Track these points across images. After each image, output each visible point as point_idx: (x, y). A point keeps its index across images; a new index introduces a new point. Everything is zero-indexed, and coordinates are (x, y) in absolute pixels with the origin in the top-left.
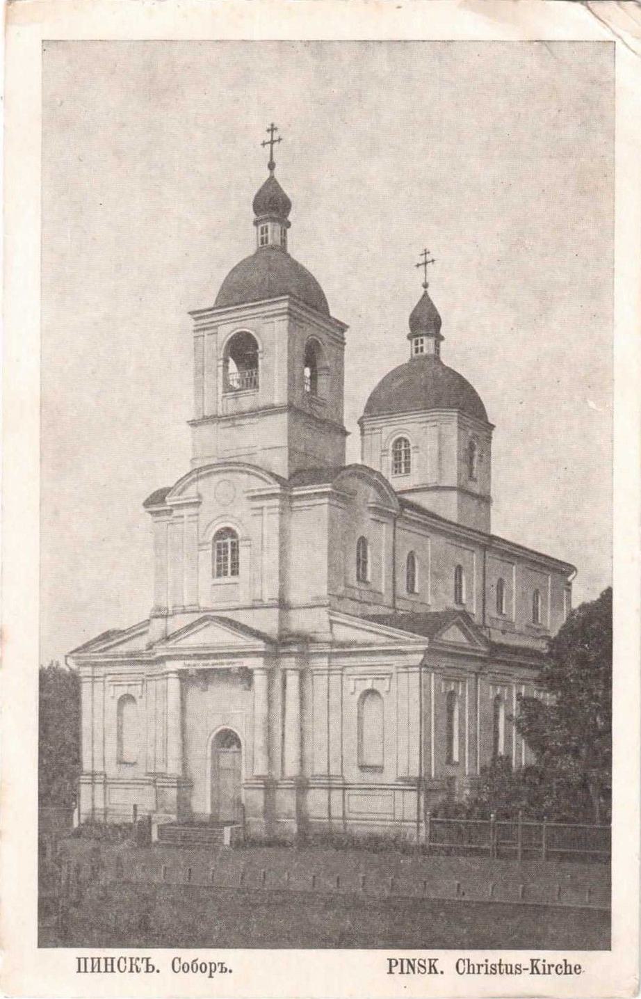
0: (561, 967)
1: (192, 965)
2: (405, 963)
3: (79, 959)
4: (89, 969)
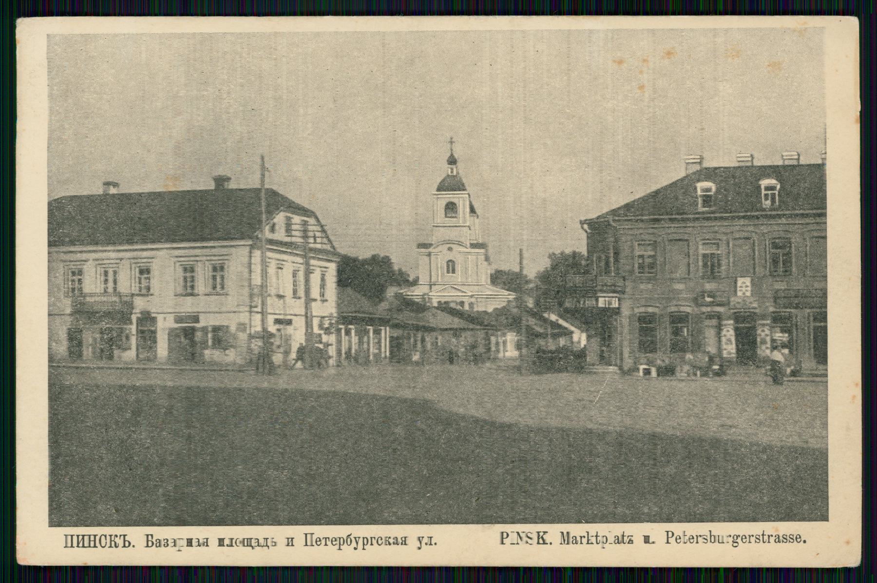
4: (75, 544)
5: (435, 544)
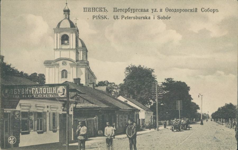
1: (208, 10)
2: (97, 17)
3: (84, 8)
4: (87, 11)
5: (157, 11)
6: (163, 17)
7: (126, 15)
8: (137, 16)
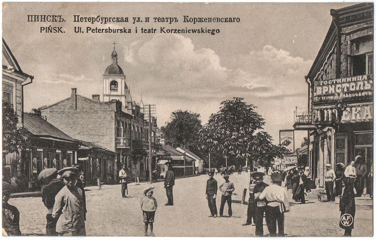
0: (223, 19)
3: (29, 16)
6: (108, 29)
7: (93, 26)
8: (110, 29)
